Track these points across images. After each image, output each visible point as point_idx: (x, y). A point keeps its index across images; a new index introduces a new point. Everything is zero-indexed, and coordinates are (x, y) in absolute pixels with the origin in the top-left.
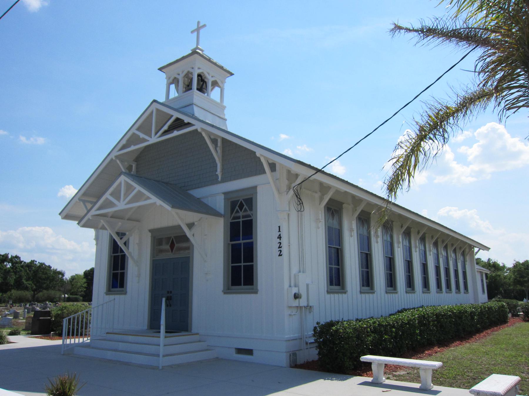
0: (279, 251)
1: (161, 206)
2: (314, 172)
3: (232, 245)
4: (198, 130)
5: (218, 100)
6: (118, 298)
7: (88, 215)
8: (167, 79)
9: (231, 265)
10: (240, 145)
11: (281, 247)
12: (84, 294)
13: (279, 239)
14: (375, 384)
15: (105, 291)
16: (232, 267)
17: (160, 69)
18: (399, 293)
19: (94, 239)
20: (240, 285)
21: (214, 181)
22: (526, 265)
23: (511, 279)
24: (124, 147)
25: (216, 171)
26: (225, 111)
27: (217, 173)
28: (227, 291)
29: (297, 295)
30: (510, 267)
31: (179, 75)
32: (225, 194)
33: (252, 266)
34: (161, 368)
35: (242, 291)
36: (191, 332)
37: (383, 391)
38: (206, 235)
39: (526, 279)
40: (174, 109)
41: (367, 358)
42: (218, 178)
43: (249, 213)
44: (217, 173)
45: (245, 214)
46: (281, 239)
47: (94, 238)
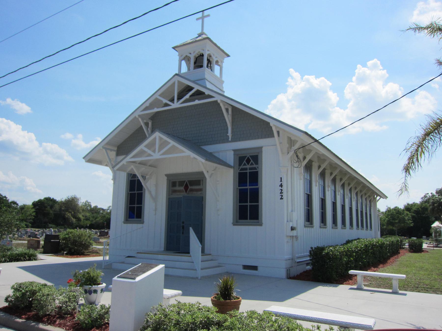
0: (280, 196)
1: (194, 158)
2: (313, 141)
3: (131, 194)
4: (218, 101)
5: (219, 76)
6: (133, 227)
7: (124, 160)
8: (179, 56)
9: (239, 204)
10: (256, 117)
11: (282, 193)
12: (32, 221)
13: (281, 187)
14: (360, 289)
15: (123, 220)
16: (239, 205)
17: (174, 48)
18: (315, 227)
19: (112, 179)
20: (247, 219)
21: (225, 140)
22: (397, 210)
23: (386, 220)
24: (146, 109)
25: (227, 133)
26: (223, 84)
27: (228, 135)
28: (235, 223)
29: (293, 228)
30: (383, 211)
31: (190, 54)
32: (235, 151)
33: (258, 205)
34: (199, 278)
35: (243, 223)
36: (204, 253)
37: (371, 293)
38: (218, 181)
39: (397, 221)
40: (192, 81)
41: (352, 272)
42: (229, 139)
43: (255, 166)
44: (228, 135)
45: (252, 166)
46: (282, 187)
47: (112, 178)
